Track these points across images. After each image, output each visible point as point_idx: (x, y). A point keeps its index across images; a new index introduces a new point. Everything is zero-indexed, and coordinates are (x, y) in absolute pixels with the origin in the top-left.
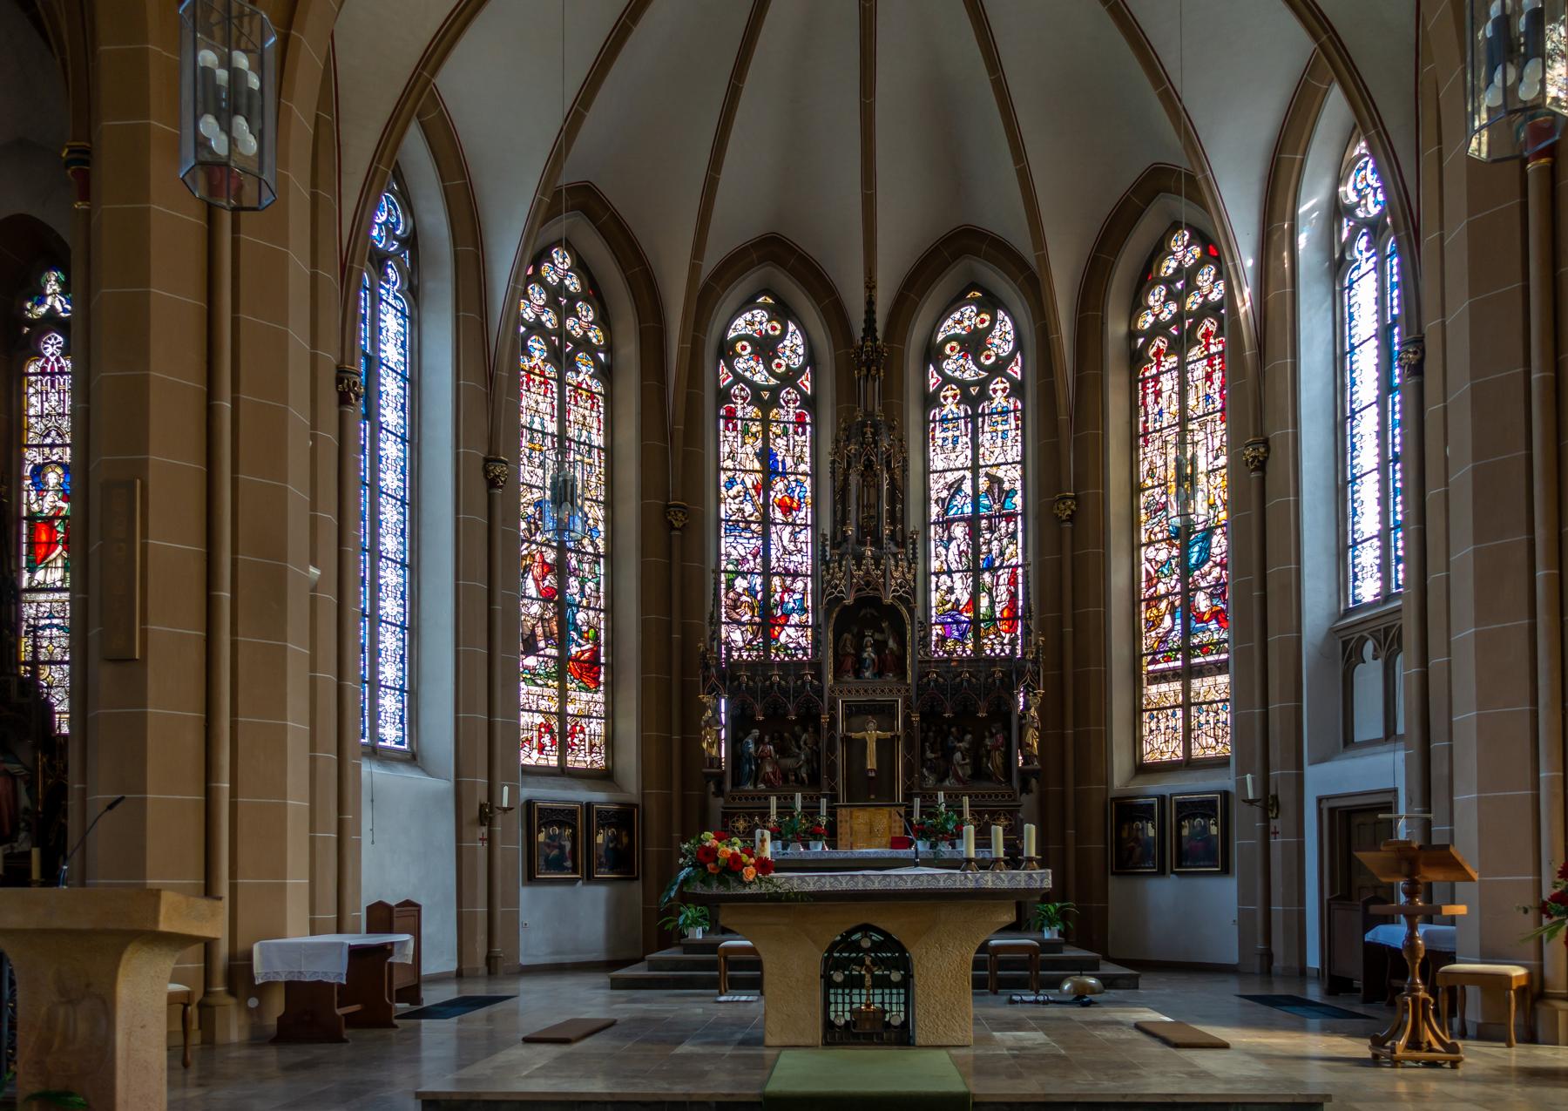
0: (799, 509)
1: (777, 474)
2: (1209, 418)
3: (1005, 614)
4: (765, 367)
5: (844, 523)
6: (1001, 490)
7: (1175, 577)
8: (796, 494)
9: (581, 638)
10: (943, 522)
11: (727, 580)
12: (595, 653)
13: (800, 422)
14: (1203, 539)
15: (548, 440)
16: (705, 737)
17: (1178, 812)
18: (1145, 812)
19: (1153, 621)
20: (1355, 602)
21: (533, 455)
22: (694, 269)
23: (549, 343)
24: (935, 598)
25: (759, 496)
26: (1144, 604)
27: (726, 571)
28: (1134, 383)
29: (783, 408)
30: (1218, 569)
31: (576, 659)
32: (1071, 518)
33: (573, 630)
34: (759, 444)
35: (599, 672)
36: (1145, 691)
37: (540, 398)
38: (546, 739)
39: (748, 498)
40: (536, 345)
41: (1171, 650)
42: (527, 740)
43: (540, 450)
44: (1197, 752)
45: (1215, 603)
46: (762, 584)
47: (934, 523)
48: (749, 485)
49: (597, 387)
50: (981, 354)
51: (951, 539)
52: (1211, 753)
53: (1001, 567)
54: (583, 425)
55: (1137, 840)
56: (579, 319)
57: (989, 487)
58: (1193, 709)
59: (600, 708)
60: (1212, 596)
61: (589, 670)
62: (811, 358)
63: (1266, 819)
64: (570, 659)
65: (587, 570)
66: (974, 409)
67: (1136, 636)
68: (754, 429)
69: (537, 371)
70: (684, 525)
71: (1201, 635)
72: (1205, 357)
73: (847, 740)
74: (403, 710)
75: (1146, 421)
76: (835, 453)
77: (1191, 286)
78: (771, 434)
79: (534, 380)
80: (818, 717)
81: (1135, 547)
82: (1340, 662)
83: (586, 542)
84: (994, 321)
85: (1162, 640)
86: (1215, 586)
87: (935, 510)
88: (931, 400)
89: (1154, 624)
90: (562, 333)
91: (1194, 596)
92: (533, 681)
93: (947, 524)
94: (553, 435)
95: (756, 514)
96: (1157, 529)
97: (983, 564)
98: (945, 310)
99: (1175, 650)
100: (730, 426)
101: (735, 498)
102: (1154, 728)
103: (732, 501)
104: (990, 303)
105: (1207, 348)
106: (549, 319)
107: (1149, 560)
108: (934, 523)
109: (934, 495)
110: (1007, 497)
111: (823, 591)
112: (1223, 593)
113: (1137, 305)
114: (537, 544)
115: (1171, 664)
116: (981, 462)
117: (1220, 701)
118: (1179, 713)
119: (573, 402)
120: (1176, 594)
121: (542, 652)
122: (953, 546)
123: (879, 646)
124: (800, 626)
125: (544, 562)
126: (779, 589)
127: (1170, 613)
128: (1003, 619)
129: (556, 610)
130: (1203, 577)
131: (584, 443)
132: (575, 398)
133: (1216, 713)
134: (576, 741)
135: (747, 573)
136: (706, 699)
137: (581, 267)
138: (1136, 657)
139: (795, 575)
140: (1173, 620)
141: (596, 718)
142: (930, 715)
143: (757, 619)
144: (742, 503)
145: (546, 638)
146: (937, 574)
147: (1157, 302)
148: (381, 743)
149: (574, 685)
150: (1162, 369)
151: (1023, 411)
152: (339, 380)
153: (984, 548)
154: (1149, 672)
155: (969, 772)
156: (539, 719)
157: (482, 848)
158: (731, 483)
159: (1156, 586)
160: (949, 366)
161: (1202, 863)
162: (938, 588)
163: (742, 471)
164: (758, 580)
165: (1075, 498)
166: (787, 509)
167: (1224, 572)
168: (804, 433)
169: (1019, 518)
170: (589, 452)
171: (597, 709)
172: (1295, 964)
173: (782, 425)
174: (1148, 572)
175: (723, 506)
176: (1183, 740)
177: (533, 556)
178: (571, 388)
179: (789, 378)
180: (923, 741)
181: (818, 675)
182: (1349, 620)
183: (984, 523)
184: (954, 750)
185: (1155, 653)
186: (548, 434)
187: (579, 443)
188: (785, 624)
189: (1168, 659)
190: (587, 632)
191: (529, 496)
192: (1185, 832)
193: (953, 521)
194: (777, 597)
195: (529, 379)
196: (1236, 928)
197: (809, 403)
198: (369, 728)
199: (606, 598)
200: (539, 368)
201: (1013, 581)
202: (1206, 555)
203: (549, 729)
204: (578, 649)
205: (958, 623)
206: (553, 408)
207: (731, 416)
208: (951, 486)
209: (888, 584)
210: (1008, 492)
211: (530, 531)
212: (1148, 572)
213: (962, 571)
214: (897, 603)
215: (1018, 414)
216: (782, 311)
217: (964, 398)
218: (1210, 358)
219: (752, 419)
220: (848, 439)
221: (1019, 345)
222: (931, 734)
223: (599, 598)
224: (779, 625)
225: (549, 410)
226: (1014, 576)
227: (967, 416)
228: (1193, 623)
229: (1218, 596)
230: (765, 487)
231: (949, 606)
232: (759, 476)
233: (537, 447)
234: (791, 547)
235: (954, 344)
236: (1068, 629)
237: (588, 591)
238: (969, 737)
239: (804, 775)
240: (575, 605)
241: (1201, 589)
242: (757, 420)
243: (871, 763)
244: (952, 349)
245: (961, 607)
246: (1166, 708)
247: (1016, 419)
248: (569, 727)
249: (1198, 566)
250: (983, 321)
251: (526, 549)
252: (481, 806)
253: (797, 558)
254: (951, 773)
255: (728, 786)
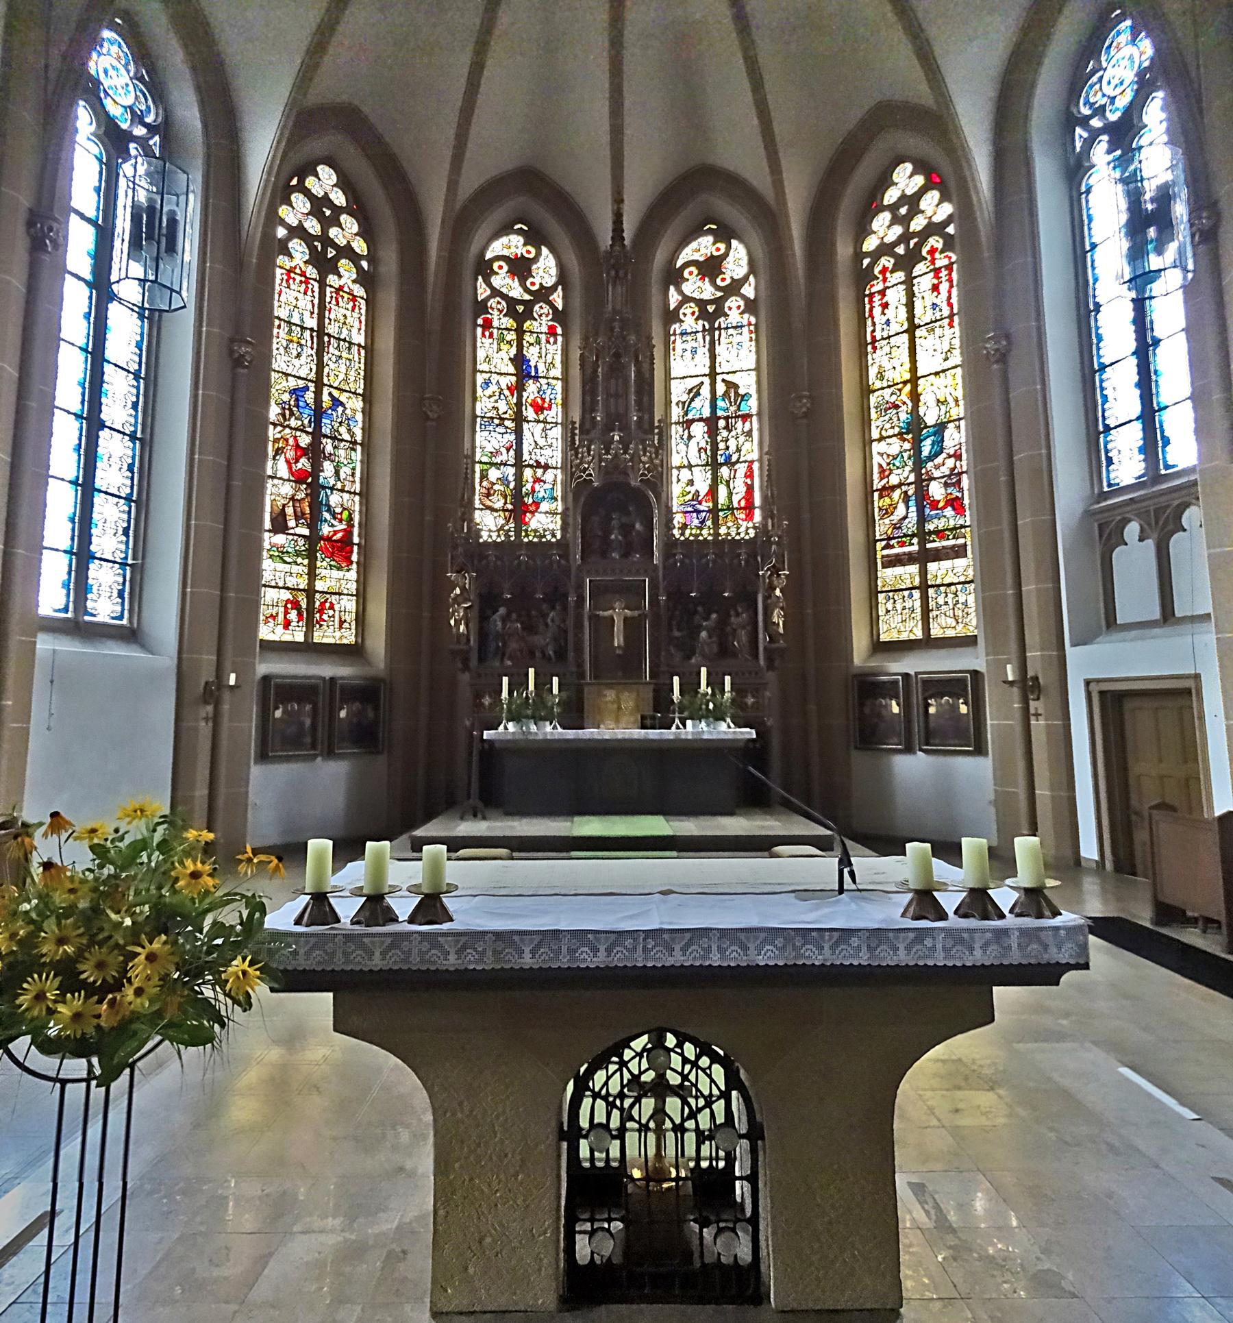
0: (550, 408)
1: (530, 377)
2: (937, 324)
3: (743, 503)
4: (520, 285)
5: (593, 410)
6: (737, 394)
7: (908, 469)
8: (547, 395)
9: (335, 518)
10: (683, 422)
11: (482, 471)
12: (348, 533)
13: (552, 332)
14: (934, 434)
15: (307, 334)
16: (453, 614)
17: (924, 690)
18: (889, 689)
19: (886, 510)
20: (1110, 485)
21: (291, 346)
22: (453, 185)
23: (312, 249)
24: (676, 490)
25: (513, 395)
26: (876, 495)
27: (481, 462)
28: (861, 299)
29: (536, 320)
30: (952, 460)
31: (328, 539)
32: (806, 415)
33: (327, 511)
34: (513, 351)
35: (352, 552)
36: (879, 574)
37: (301, 296)
38: (293, 615)
39: (502, 397)
40: (298, 249)
41: (905, 536)
42: (272, 615)
43: (298, 343)
44: (936, 632)
45: (949, 491)
46: (515, 474)
47: (676, 423)
48: (504, 386)
49: (359, 291)
50: (717, 277)
51: (690, 437)
52: (951, 633)
53: (738, 461)
54: (344, 323)
55: (879, 716)
56: (343, 230)
57: (726, 392)
58: (931, 591)
59: (353, 587)
60: (946, 485)
61: (341, 550)
62: (563, 279)
63: (1025, 701)
64: (322, 538)
65: (343, 455)
66: (712, 324)
67: (870, 523)
68: (509, 338)
69: (298, 271)
70: (439, 417)
71: (936, 521)
72: (931, 271)
73: (594, 618)
74: (124, 583)
75: (874, 331)
76: (584, 348)
77: (915, 211)
78: (524, 342)
79: (294, 279)
80: (566, 596)
81: (867, 442)
82: (1098, 544)
83: (343, 430)
84: (729, 247)
85: (896, 526)
86: (949, 476)
87: (676, 412)
88: (672, 317)
89: (888, 512)
90: (327, 241)
91: (928, 486)
92: (281, 558)
93: (688, 424)
94: (312, 330)
95: (510, 412)
96: (888, 426)
97: (721, 460)
98: (684, 240)
99: (908, 536)
100: (487, 334)
101: (490, 397)
102: (890, 608)
103: (487, 400)
104: (725, 234)
105: (933, 262)
106: (313, 226)
107: (881, 454)
108: (676, 423)
109: (674, 399)
110: (742, 400)
111: (572, 474)
112: (959, 482)
113: (863, 230)
114: (291, 428)
115: (906, 549)
116: (718, 370)
117: (959, 583)
118: (917, 594)
119: (334, 302)
120: (909, 484)
121: (291, 531)
122: (693, 442)
123: (626, 529)
124: (550, 513)
125: (297, 446)
126: (531, 480)
127: (903, 501)
128: (741, 508)
129: (309, 491)
130: (937, 467)
131: (345, 340)
132: (337, 299)
133: (956, 594)
134: (325, 617)
135: (500, 465)
136: (452, 576)
137: (344, 183)
138: (871, 543)
139: (546, 467)
140: (908, 508)
141: (348, 595)
142: (677, 596)
143: (510, 507)
144: (496, 401)
145: (297, 518)
146: (678, 468)
147: (883, 229)
148: (87, 618)
149: (325, 564)
150: (887, 284)
151: (756, 325)
152: (30, 224)
153: (722, 446)
154: (883, 557)
155: (715, 649)
156: (286, 595)
157: (205, 729)
158: (487, 384)
159: (888, 477)
160: (687, 288)
161: (952, 742)
162: (679, 480)
163: (498, 374)
164: (511, 471)
165: (810, 397)
166: (538, 409)
167: (958, 463)
168: (555, 342)
169: (755, 419)
170: (349, 349)
171: (348, 586)
172: (1068, 853)
173: (535, 335)
174: (880, 466)
175: (478, 404)
176: (922, 619)
177: (287, 440)
178: (333, 290)
179: (543, 294)
180: (671, 618)
181: (565, 555)
182: (1155, 489)
183: (722, 423)
184: (699, 628)
185: (889, 539)
186: (306, 328)
187: (339, 339)
188: (536, 511)
189: (902, 544)
190: (341, 514)
191: (284, 383)
192: (932, 710)
193: (693, 421)
194: (529, 486)
195: (289, 277)
196: (993, 810)
197: (559, 316)
198: (75, 602)
199: (361, 483)
200: (300, 269)
201: (749, 474)
202: (939, 449)
203: (296, 605)
204: (331, 529)
205: (698, 512)
206: (313, 306)
207: (488, 324)
208: (690, 391)
209: (636, 467)
210: (743, 396)
211: (283, 415)
212: (880, 466)
213: (702, 466)
214: (644, 488)
215: (752, 328)
216: (535, 237)
217: (703, 315)
218: (937, 271)
219: (507, 329)
220: (597, 334)
221: (753, 268)
222: (677, 613)
223: (354, 482)
224: (530, 512)
225: (309, 307)
226: (750, 469)
227: (704, 330)
228: (927, 511)
229: (953, 485)
230: (519, 388)
231: (689, 497)
232: (514, 379)
233: (295, 339)
234: (542, 442)
235: (692, 269)
236: (806, 516)
237: (342, 475)
238: (714, 616)
239: (551, 653)
240: (329, 488)
241: (935, 479)
242: (511, 330)
243: (618, 640)
244: (691, 273)
245: (700, 498)
246: (902, 590)
247: (751, 332)
248: (317, 604)
249: (931, 458)
250: (718, 249)
251: (280, 432)
252: (207, 683)
253: (548, 452)
254: (698, 651)
255: (474, 662)
